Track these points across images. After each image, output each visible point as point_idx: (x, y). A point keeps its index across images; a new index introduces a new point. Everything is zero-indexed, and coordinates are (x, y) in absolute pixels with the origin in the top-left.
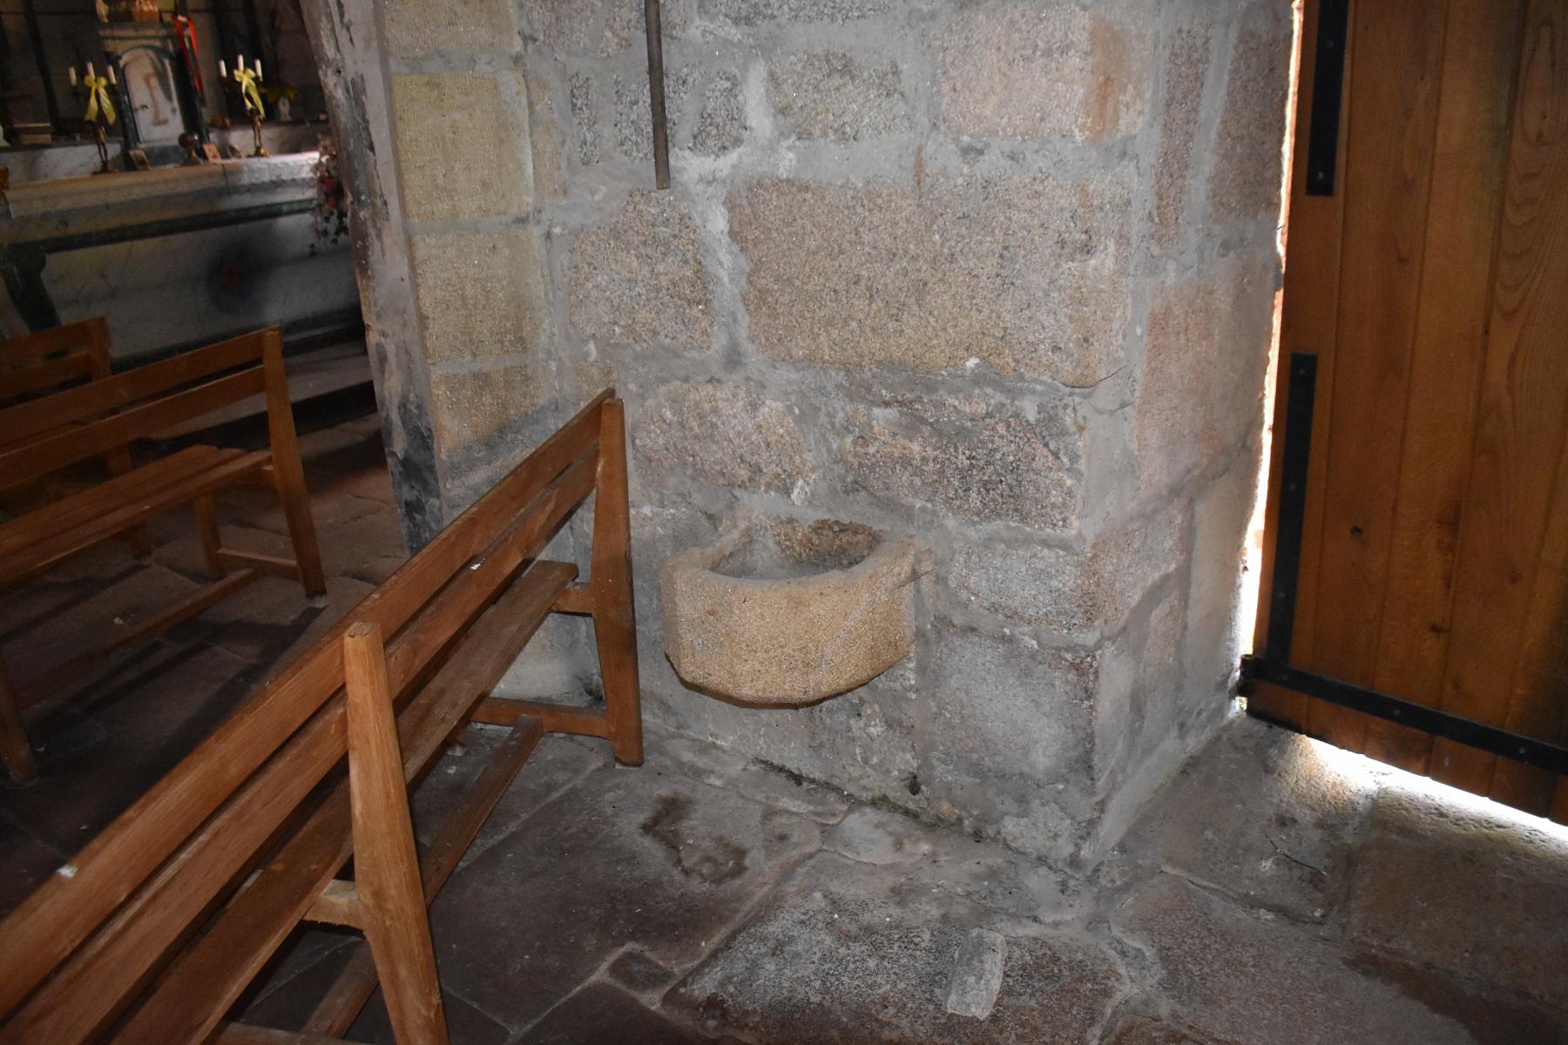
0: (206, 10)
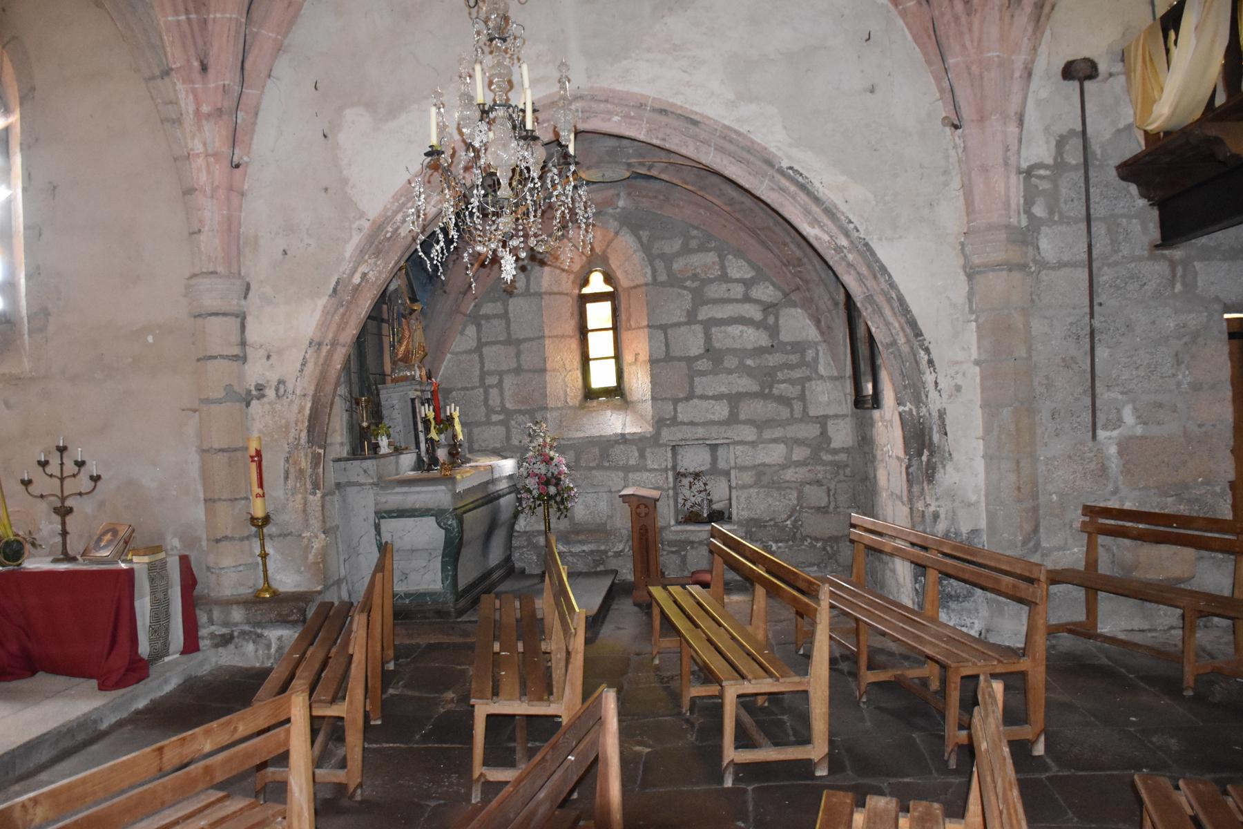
0: (591, 359)
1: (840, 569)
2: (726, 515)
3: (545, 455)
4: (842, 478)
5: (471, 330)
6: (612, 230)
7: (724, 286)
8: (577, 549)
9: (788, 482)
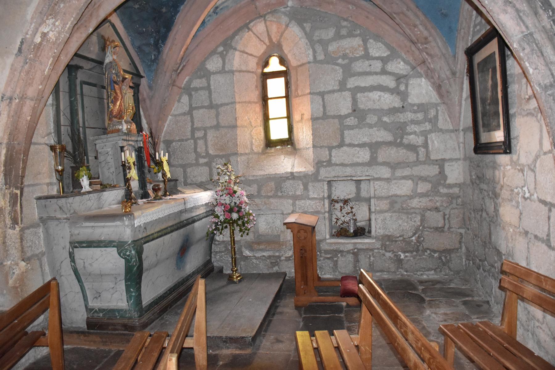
0: (270, 119)
1: (452, 273)
2: (367, 231)
3: (230, 189)
4: (454, 205)
5: (185, 99)
6: (284, 23)
7: (367, 63)
8: (258, 255)
9: (413, 208)
